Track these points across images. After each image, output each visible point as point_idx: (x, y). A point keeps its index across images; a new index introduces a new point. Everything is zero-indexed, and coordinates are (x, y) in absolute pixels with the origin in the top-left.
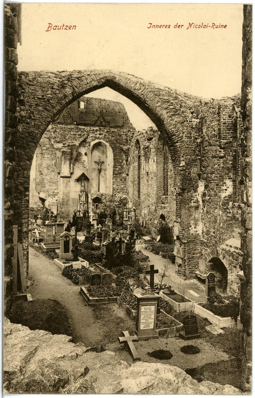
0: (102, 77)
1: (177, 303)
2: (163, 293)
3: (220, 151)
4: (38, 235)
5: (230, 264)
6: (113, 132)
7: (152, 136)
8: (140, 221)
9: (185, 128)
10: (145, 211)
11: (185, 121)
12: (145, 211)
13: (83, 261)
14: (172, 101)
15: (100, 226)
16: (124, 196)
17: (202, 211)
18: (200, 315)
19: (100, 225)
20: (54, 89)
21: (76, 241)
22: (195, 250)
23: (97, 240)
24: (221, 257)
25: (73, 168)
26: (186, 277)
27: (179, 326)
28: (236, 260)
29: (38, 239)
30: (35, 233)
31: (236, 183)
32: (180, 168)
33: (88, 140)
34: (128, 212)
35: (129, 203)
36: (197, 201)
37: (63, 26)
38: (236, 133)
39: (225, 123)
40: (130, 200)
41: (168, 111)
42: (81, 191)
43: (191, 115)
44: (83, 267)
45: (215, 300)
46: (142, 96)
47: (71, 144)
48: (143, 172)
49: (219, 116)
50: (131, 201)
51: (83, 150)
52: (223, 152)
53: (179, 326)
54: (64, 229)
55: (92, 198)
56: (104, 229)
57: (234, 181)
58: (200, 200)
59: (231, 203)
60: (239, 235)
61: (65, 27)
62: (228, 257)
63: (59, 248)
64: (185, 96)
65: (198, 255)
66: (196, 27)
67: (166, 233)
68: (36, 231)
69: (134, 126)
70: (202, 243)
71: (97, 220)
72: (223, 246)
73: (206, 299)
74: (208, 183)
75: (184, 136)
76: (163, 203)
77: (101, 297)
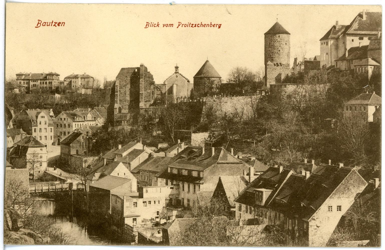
37: (52, 23)
61: (53, 24)
66: (155, 25)
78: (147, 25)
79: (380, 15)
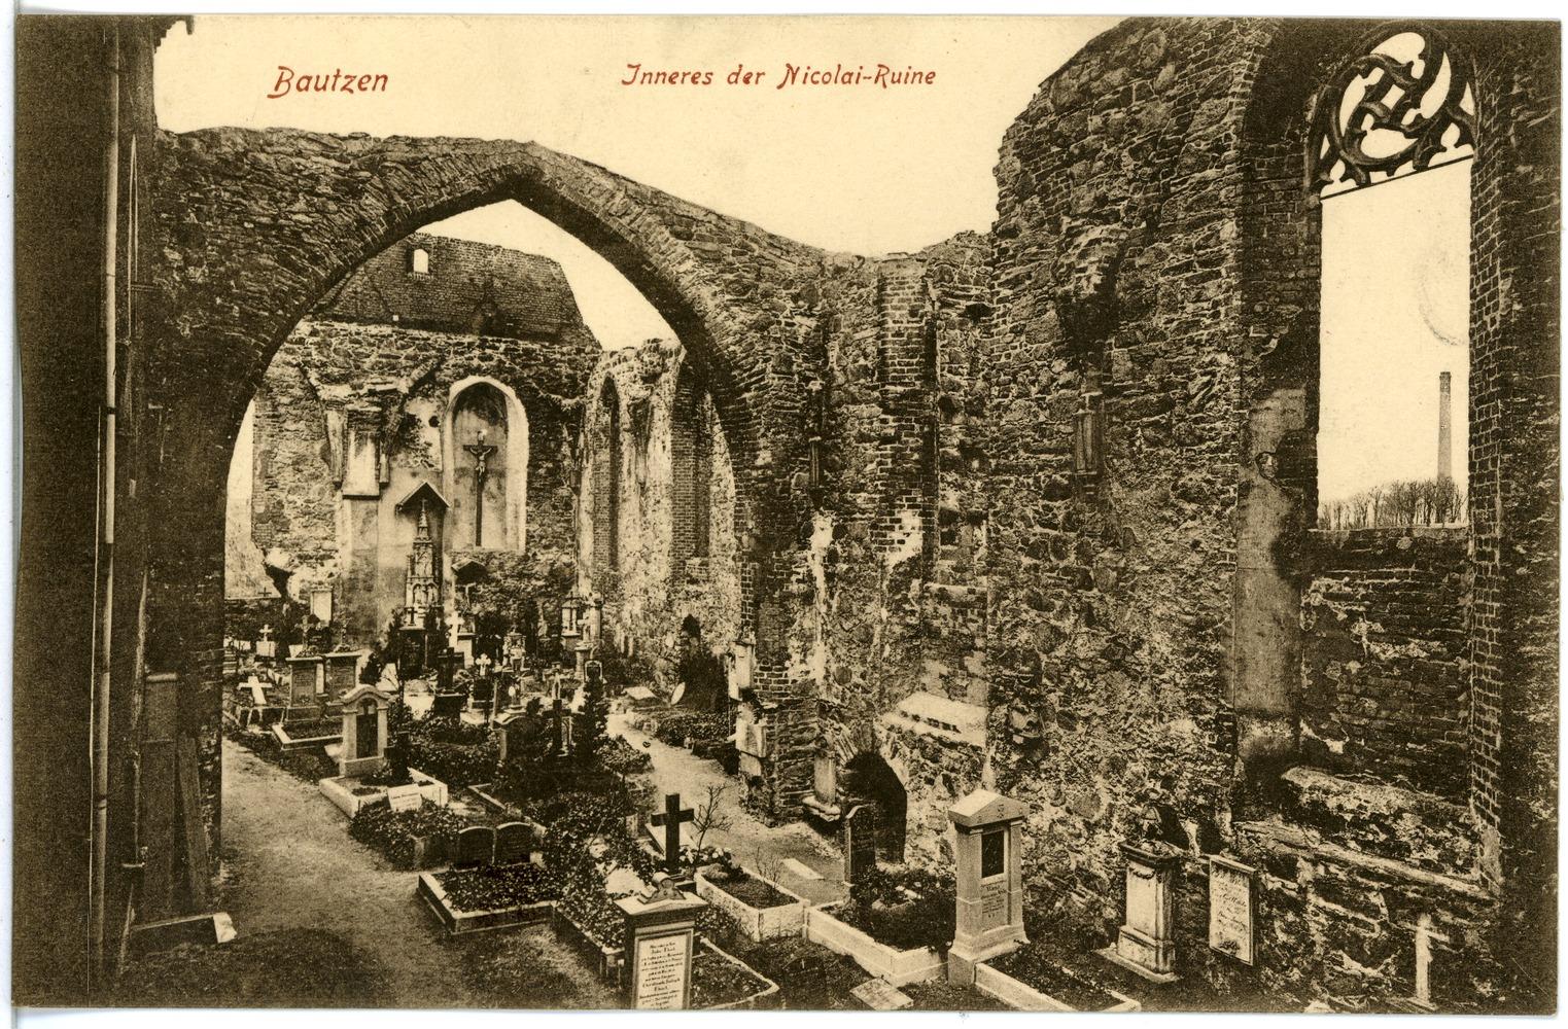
0: (495, 166)
1: (754, 911)
2: (708, 878)
3: (884, 421)
4: (259, 698)
5: (913, 773)
6: (527, 352)
7: (659, 369)
8: (616, 640)
9: (773, 345)
10: (634, 607)
11: (772, 323)
12: (634, 607)
13: (428, 783)
14: (731, 259)
15: (484, 660)
16: (565, 559)
17: (824, 609)
18: (829, 945)
19: (484, 656)
20: (318, 195)
21: (399, 713)
22: (801, 732)
23: (475, 706)
24: (885, 751)
25: (390, 469)
26: (776, 819)
27: (765, 993)
28: (935, 761)
29: (260, 709)
30: (250, 689)
31: (930, 522)
32: (754, 474)
33: (440, 377)
34: (577, 609)
35: (582, 581)
36: (810, 578)
38: (933, 365)
39: (898, 334)
40: (582, 573)
41: (717, 289)
42: (416, 546)
43: (790, 305)
44: (428, 805)
45: (875, 891)
46: (631, 238)
47: (379, 388)
48: (628, 483)
49: (881, 309)
50: (587, 576)
51: (423, 409)
52: (891, 424)
53: (765, 993)
54: (358, 671)
55: (455, 566)
56: (498, 668)
57: (925, 514)
58: (819, 572)
59: (916, 583)
60: (940, 683)
61: (341, 82)
62: (907, 750)
63: (338, 741)
64: (771, 245)
65: (812, 745)
66: (816, 78)
67: (701, 672)
68: (253, 682)
69: (598, 335)
70: (824, 710)
71: (473, 638)
72: (893, 718)
73: (847, 892)
74: (845, 520)
75: (769, 369)
76: (693, 581)
77: (495, 907)
78: (930, 78)
79: (1557, 26)
